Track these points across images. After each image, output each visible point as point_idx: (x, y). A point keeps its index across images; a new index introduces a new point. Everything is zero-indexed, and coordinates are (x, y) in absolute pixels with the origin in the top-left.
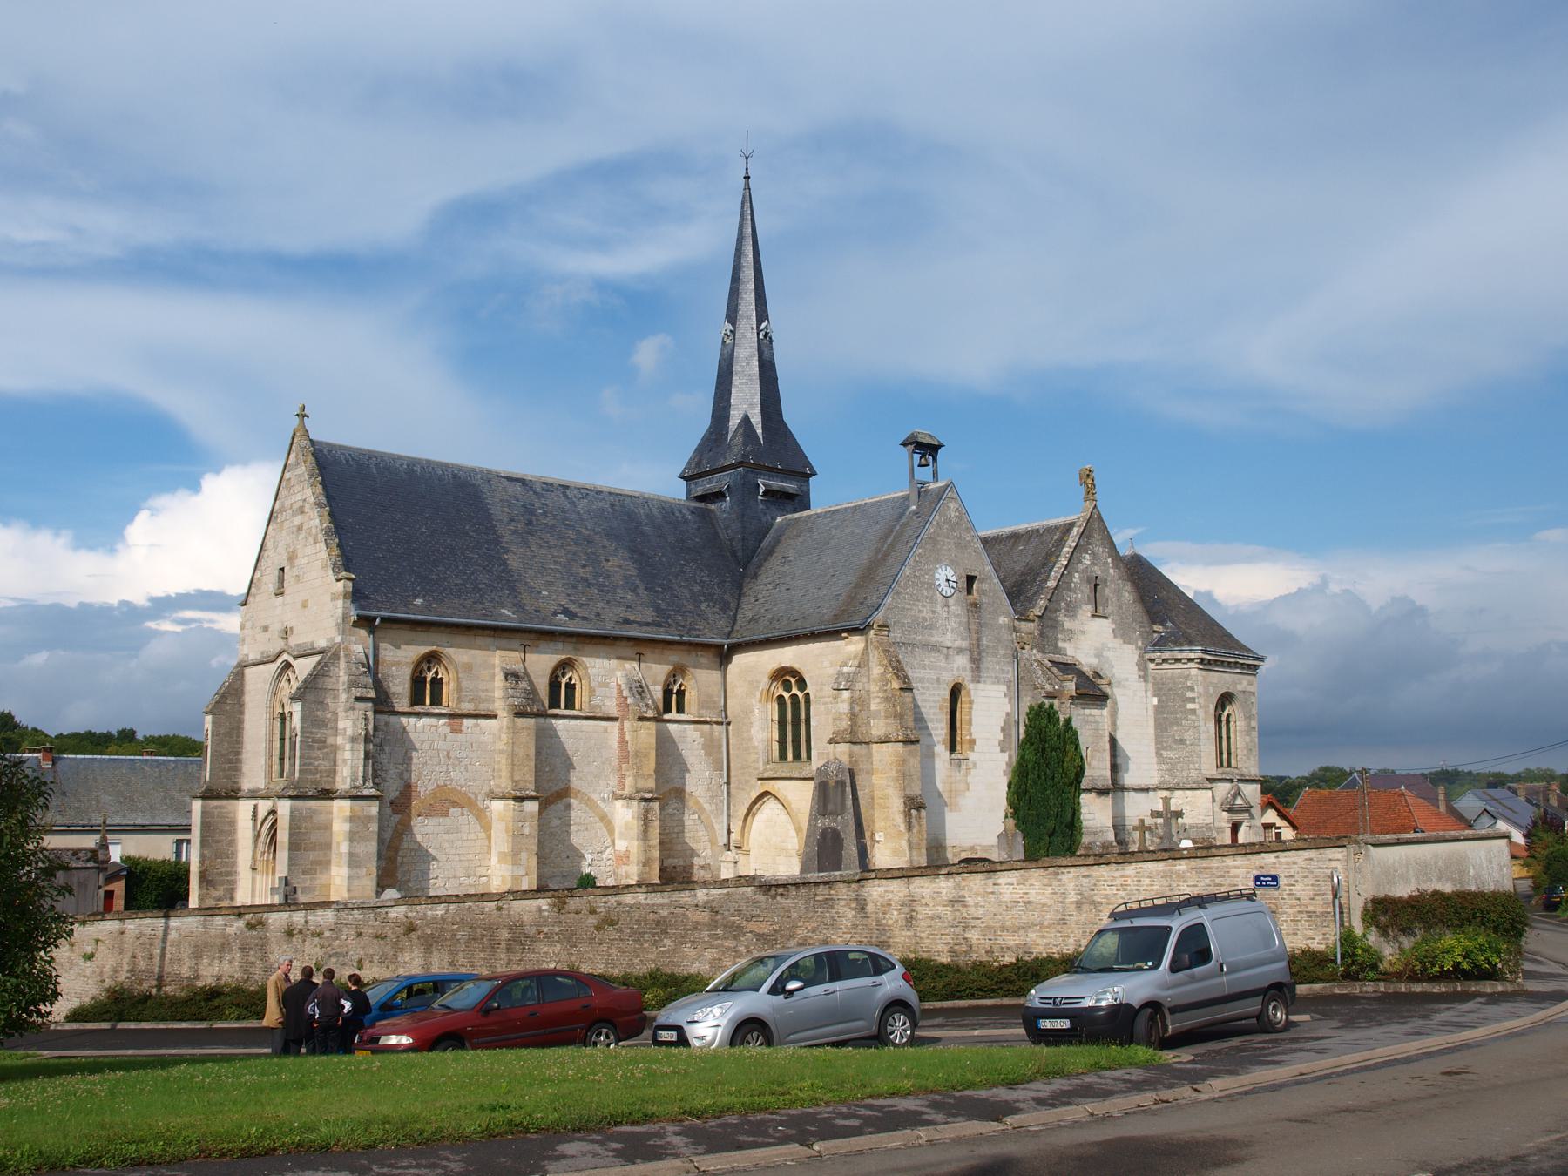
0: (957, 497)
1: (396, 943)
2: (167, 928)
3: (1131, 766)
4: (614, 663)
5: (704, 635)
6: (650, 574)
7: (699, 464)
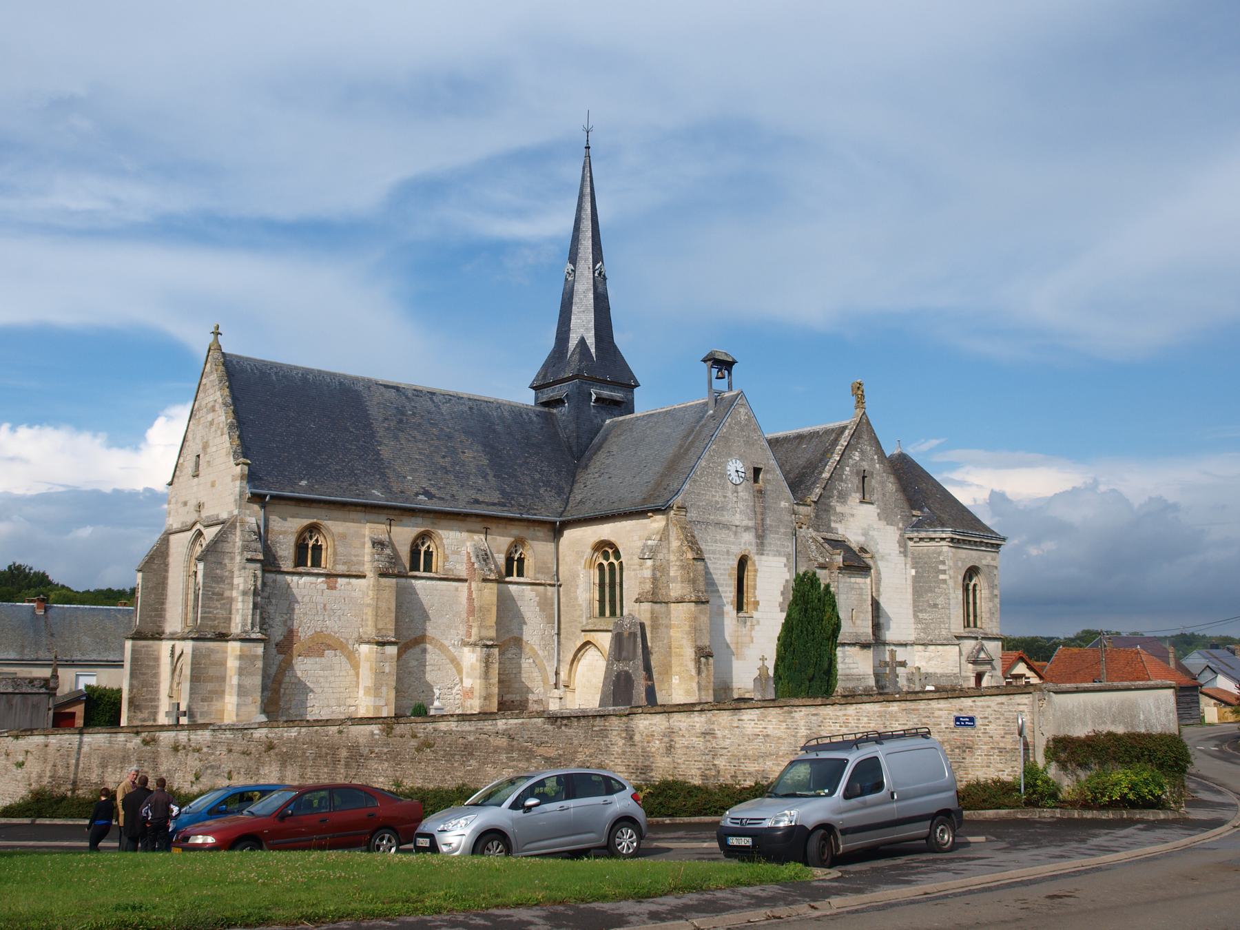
0: (746, 404)
1: (258, 759)
2: (81, 742)
3: (893, 625)
4: (465, 535)
5: (541, 514)
6: (499, 464)
7: (545, 377)
